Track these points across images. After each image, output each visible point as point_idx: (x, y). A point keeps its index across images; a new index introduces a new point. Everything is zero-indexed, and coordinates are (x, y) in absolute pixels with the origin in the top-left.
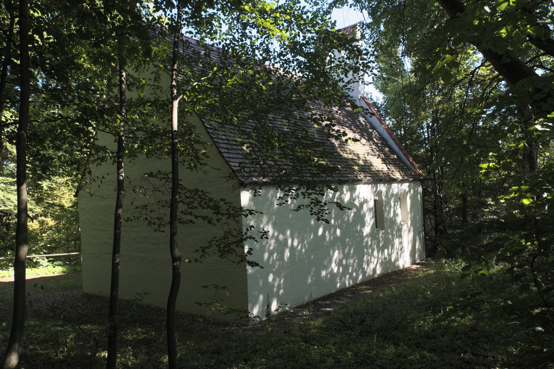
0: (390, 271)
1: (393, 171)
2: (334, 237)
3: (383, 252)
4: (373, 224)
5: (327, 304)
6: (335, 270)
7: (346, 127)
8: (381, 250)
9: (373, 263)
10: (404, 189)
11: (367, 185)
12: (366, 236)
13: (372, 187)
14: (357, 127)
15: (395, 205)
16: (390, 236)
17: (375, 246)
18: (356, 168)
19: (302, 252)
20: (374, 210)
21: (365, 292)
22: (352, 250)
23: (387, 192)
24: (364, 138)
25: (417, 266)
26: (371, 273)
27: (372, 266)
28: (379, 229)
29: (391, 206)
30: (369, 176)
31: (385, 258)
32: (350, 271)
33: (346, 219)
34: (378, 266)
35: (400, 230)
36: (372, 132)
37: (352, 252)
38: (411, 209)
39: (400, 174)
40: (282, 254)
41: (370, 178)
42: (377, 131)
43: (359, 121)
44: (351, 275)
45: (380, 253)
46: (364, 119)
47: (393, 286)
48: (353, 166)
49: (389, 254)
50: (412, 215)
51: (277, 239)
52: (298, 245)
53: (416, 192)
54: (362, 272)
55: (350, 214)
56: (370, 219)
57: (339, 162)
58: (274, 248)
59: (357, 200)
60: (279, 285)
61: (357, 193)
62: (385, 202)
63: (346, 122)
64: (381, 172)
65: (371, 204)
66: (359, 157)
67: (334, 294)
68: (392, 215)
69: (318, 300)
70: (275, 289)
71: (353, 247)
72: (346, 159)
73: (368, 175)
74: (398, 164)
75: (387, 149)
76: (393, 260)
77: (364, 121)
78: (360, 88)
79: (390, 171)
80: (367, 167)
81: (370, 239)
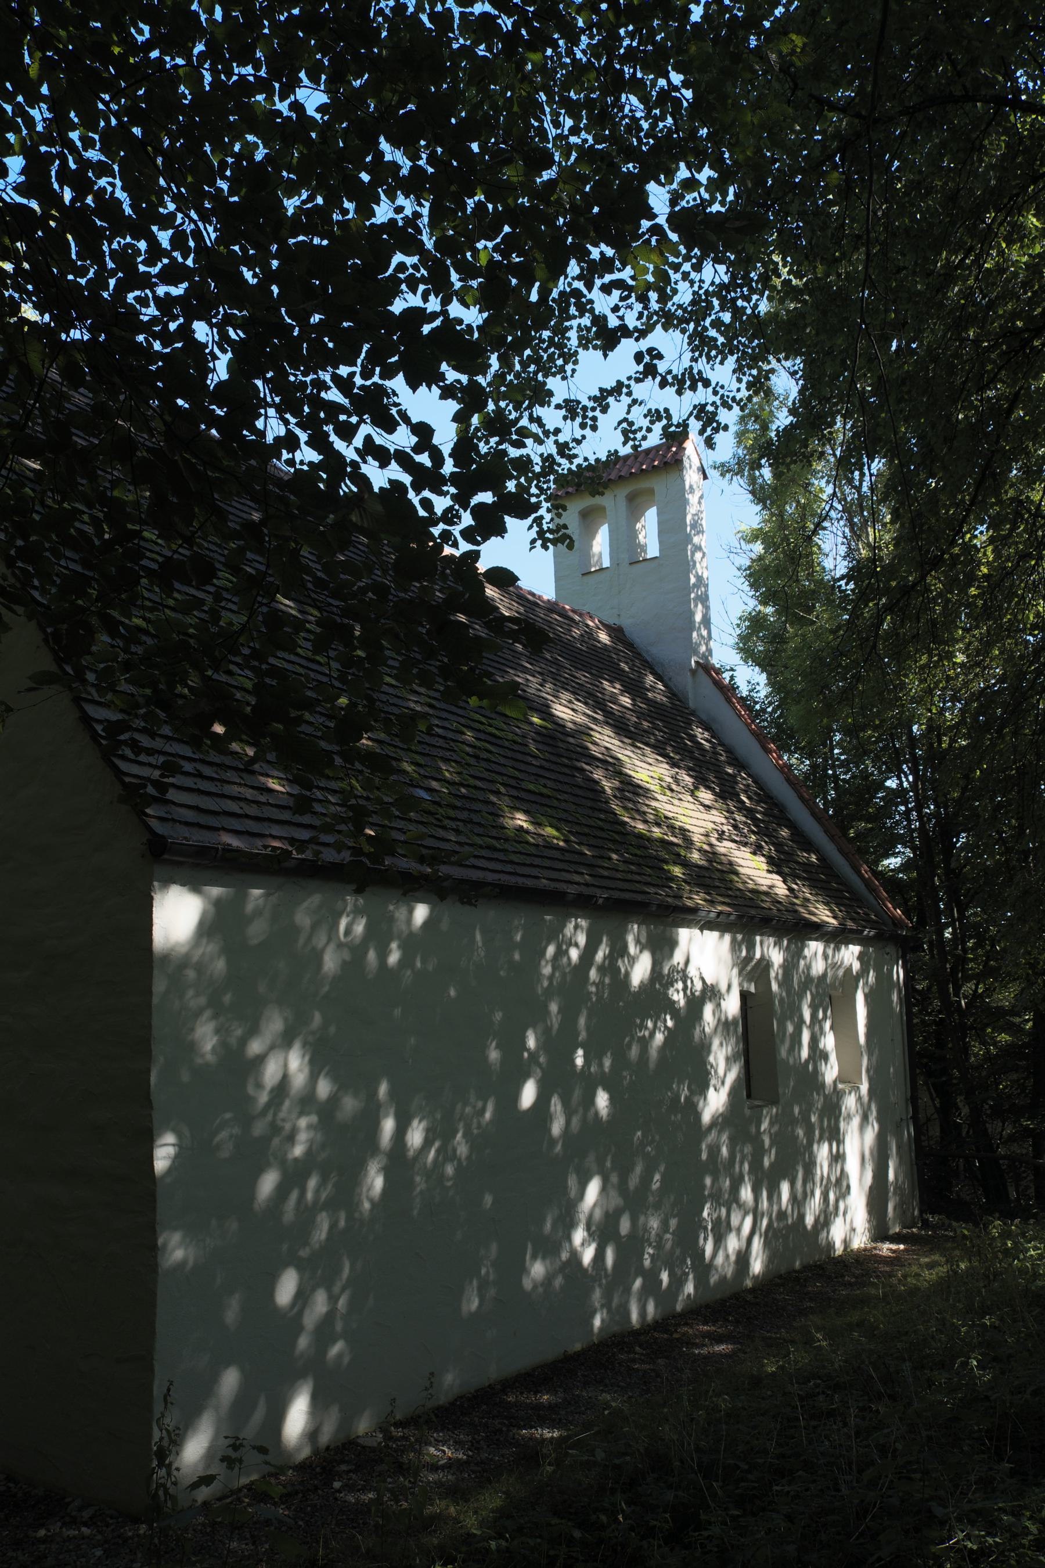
0: (797, 1264)
1: (807, 900)
2: (584, 1120)
3: (774, 1192)
4: (738, 1080)
5: (539, 1407)
6: (588, 1255)
7: (647, 744)
8: (765, 1183)
9: (739, 1230)
10: (846, 963)
11: (716, 934)
12: (714, 1123)
13: (733, 941)
14: (681, 749)
15: (814, 1016)
16: (800, 1132)
17: (746, 1166)
18: (677, 871)
19: (442, 1177)
20: (740, 1029)
21: (704, 1351)
22: (657, 1177)
23: (789, 967)
24: (708, 788)
25: (894, 1247)
26: (729, 1271)
27: (733, 1244)
28: (757, 1103)
29: (802, 1021)
30: (724, 903)
31: (782, 1215)
32: (647, 1263)
33: (634, 1052)
34: (757, 1244)
35: (832, 1109)
36: (734, 776)
37: (655, 1186)
38: (868, 1035)
39: (832, 911)
40: (353, 1176)
41: (728, 909)
42: (749, 775)
43: (693, 738)
44: (651, 1279)
45: (765, 1194)
46: (706, 735)
47: (818, 1330)
48: (667, 862)
49: (793, 1197)
50: (874, 1059)
51: (327, 1112)
52: (427, 1143)
53: (884, 981)
54: (694, 1267)
55: (652, 1034)
56: (727, 1059)
57: (614, 841)
58: (309, 1153)
59: (680, 985)
60: (329, 1317)
61: (678, 957)
62: (781, 1000)
63: (645, 731)
64: (765, 898)
65: (732, 1005)
66: (689, 843)
67: (577, 1355)
68: (805, 1053)
69: (507, 1384)
70: (303, 1342)
71: (662, 1168)
72: (640, 836)
73: (720, 899)
74: (822, 881)
75: (784, 833)
76: (809, 1220)
77: (707, 740)
78: (695, 634)
79: (796, 897)
80: (718, 875)
81: (724, 1137)
